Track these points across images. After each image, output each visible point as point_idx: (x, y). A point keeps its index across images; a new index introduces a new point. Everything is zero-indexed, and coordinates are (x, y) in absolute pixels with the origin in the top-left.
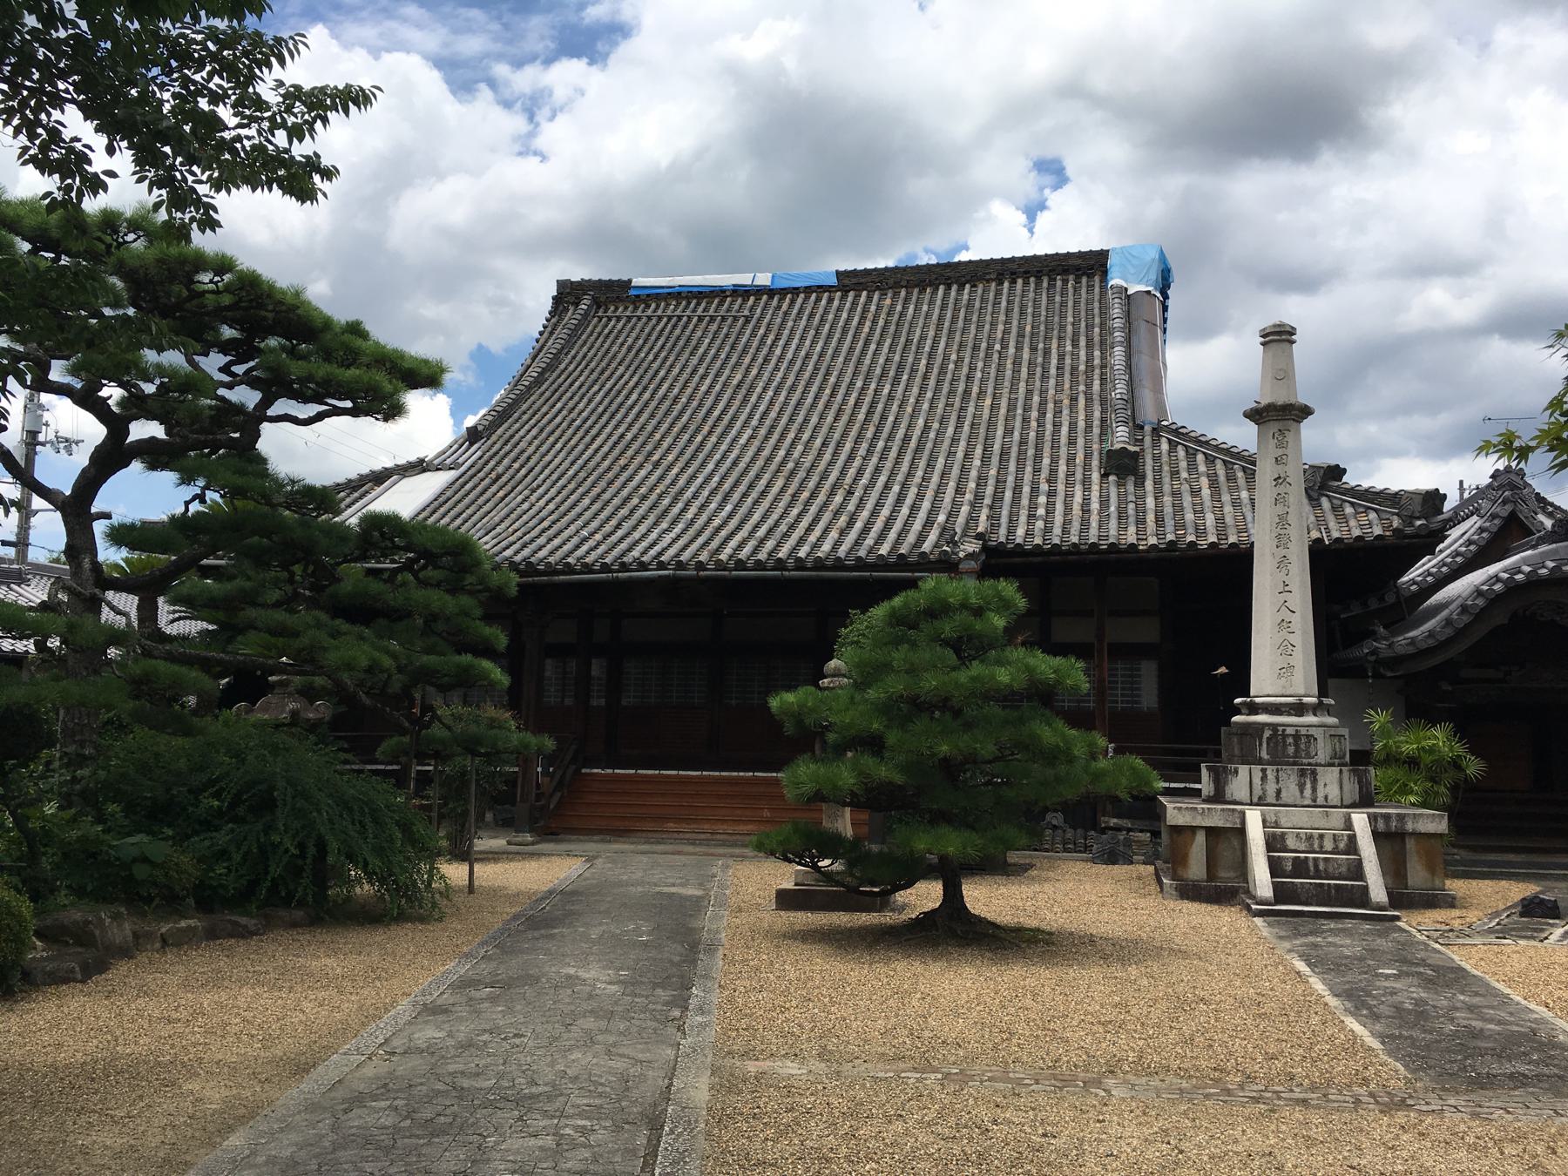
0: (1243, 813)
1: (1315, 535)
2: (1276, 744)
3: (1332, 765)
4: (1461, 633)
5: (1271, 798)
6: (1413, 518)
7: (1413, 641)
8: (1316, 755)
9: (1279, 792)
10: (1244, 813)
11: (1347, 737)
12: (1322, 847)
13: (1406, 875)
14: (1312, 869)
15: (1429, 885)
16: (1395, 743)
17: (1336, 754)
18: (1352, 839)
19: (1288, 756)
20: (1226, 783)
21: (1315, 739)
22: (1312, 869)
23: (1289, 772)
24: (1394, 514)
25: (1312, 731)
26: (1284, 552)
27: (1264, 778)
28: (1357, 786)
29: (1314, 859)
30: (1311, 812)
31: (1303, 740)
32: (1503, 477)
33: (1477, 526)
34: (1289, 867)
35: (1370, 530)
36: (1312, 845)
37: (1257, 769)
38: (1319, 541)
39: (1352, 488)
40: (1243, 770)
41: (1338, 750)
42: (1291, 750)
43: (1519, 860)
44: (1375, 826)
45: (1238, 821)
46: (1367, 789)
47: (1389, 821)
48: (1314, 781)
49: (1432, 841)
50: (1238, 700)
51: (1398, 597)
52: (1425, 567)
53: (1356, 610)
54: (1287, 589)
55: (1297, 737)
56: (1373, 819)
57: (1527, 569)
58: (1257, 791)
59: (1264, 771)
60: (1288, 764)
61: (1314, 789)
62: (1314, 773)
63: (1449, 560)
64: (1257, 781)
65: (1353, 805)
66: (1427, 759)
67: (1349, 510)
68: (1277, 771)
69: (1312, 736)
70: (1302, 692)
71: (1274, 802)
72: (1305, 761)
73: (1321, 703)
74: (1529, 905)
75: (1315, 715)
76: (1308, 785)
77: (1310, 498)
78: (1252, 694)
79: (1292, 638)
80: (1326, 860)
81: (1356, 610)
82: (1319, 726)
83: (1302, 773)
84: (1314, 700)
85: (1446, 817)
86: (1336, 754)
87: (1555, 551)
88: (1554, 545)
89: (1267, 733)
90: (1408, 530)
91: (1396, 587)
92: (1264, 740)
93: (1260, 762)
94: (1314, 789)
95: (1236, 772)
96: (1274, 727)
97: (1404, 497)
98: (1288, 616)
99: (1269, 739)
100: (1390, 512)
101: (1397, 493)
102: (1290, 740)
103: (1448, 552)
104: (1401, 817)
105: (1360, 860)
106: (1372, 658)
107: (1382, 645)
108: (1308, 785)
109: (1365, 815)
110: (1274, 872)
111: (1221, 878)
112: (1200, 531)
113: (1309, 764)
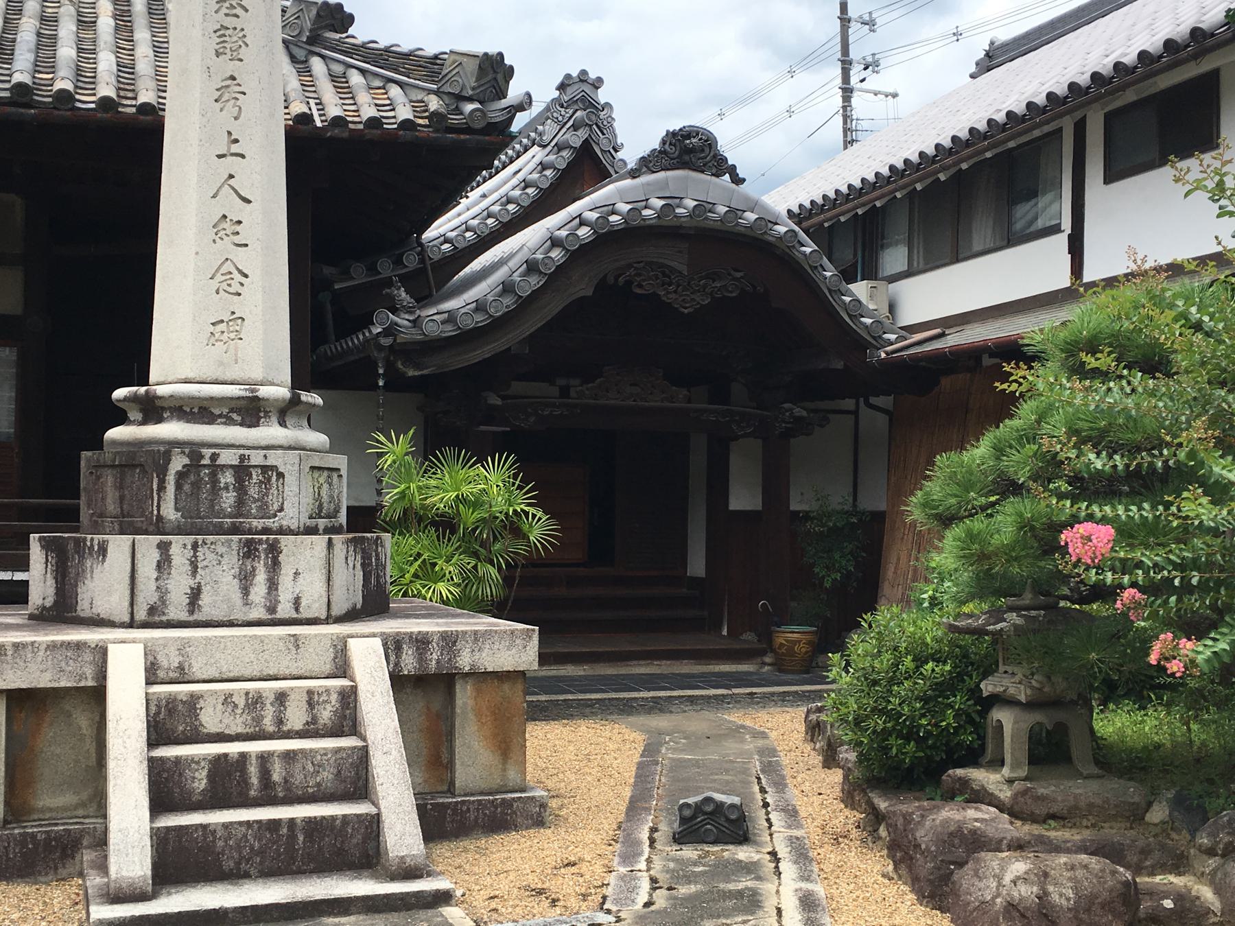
0: (102, 652)
1: (298, 108)
2: (197, 485)
3: (311, 531)
4: (525, 305)
5: (177, 611)
6: (461, 98)
7: (451, 317)
8: (281, 509)
9: (195, 595)
10: (104, 652)
11: (344, 472)
12: (280, 722)
13: (451, 762)
14: (255, 780)
15: (497, 781)
16: (420, 488)
17: (320, 507)
18: (349, 698)
19: (221, 513)
20: (80, 576)
21: (281, 475)
22: (255, 780)
23: (221, 550)
24: (430, 92)
25: (275, 458)
26: (231, 68)
27: (164, 564)
28: (360, 574)
29: (264, 758)
30: (261, 640)
31: (256, 476)
32: (576, 87)
33: (537, 160)
34: (200, 781)
35: (391, 114)
36: (258, 720)
37: (148, 545)
38: (305, 119)
39: (364, 45)
40: (119, 545)
41: (325, 498)
42: (228, 500)
43: (582, 673)
44: (397, 664)
45: (89, 671)
46: (378, 577)
47: (426, 650)
48: (274, 566)
49: (506, 687)
50: (120, 393)
51: (422, 261)
52: (463, 218)
53: (359, 276)
54: (235, 148)
55: (242, 471)
56: (393, 646)
57: (624, 207)
58: (147, 593)
59: (164, 547)
60: (220, 530)
61: (273, 585)
62: (274, 550)
63: (496, 208)
64: (147, 569)
65: (352, 616)
66: (470, 517)
67: (356, 79)
68: (195, 546)
69: (273, 468)
70: (257, 374)
71: (184, 616)
72: (257, 524)
73: (295, 401)
74: (694, 817)
75: (283, 424)
76: (261, 577)
77: (293, 59)
78: (150, 382)
79: (240, 257)
80: (289, 756)
81: (359, 276)
82: (290, 448)
83: (249, 551)
84: (283, 392)
85: (537, 633)
86: (320, 507)
87: (665, 184)
88: (662, 174)
89: (178, 463)
90: (455, 119)
91: (421, 245)
92: (171, 479)
93: (158, 526)
94: (273, 585)
95: (103, 550)
96: (193, 449)
97: (448, 63)
98: (236, 209)
99: (181, 476)
100: (423, 89)
101: (436, 57)
102: (227, 478)
103: (495, 196)
104: (450, 641)
105: (365, 750)
106: (386, 342)
107: (403, 320)
108: (261, 577)
109: (377, 642)
110: (162, 800)
111: (42, 811)
112: (84, 74)
113: (266, 531)
